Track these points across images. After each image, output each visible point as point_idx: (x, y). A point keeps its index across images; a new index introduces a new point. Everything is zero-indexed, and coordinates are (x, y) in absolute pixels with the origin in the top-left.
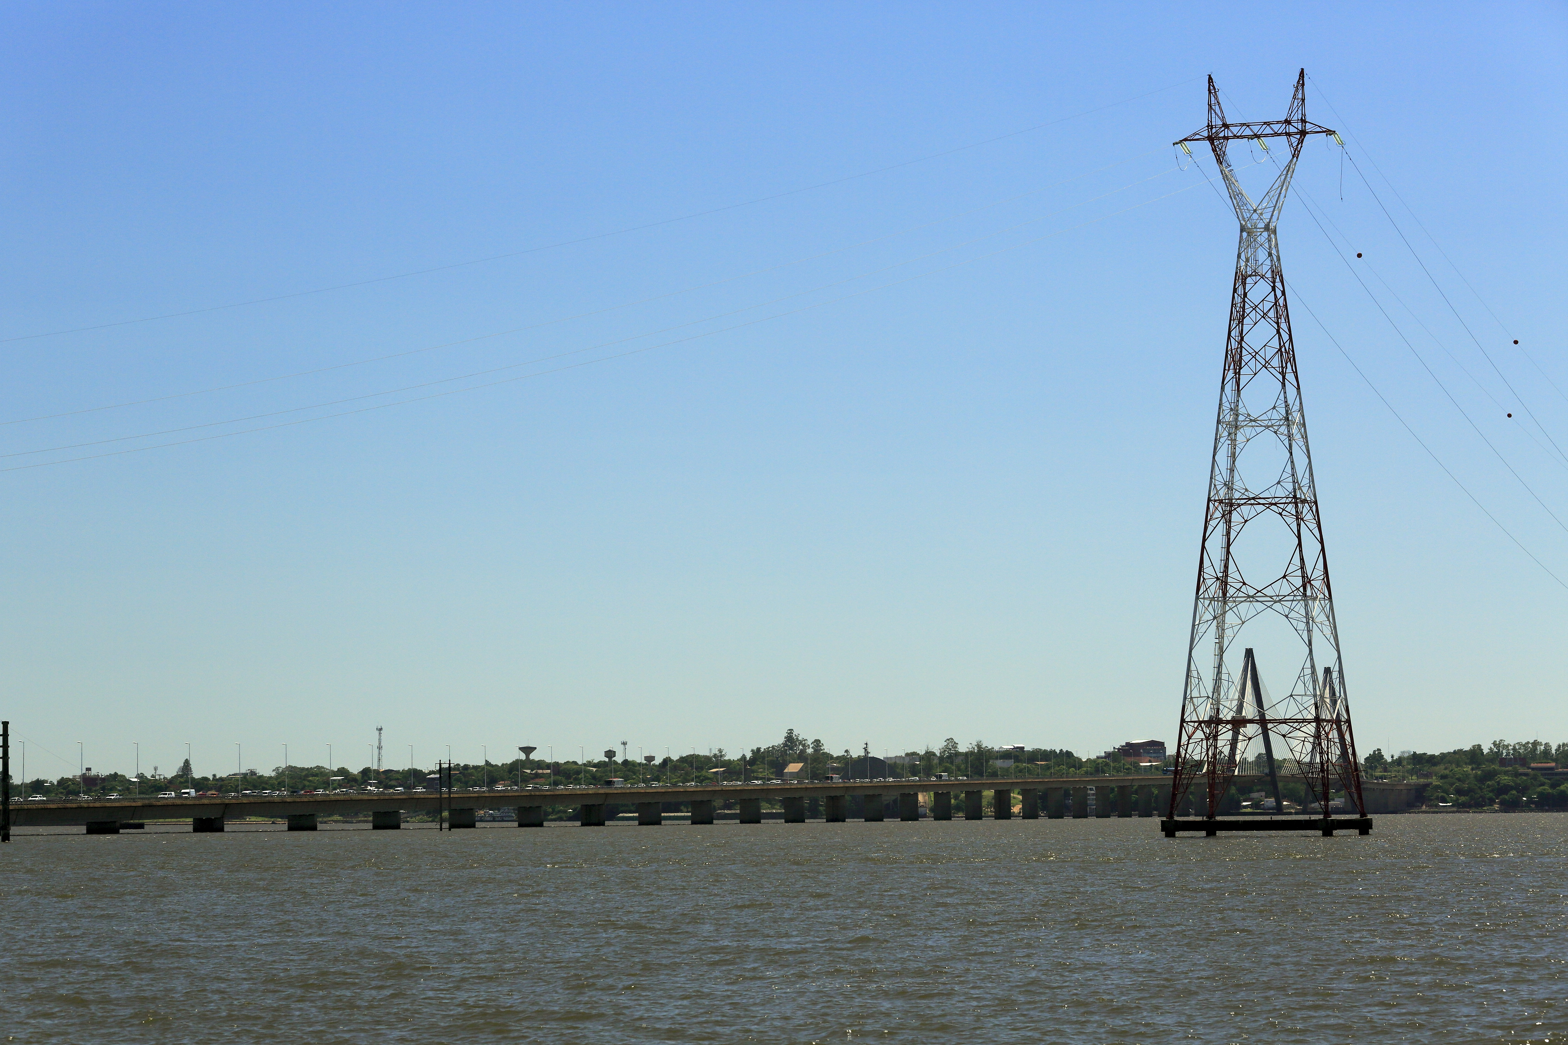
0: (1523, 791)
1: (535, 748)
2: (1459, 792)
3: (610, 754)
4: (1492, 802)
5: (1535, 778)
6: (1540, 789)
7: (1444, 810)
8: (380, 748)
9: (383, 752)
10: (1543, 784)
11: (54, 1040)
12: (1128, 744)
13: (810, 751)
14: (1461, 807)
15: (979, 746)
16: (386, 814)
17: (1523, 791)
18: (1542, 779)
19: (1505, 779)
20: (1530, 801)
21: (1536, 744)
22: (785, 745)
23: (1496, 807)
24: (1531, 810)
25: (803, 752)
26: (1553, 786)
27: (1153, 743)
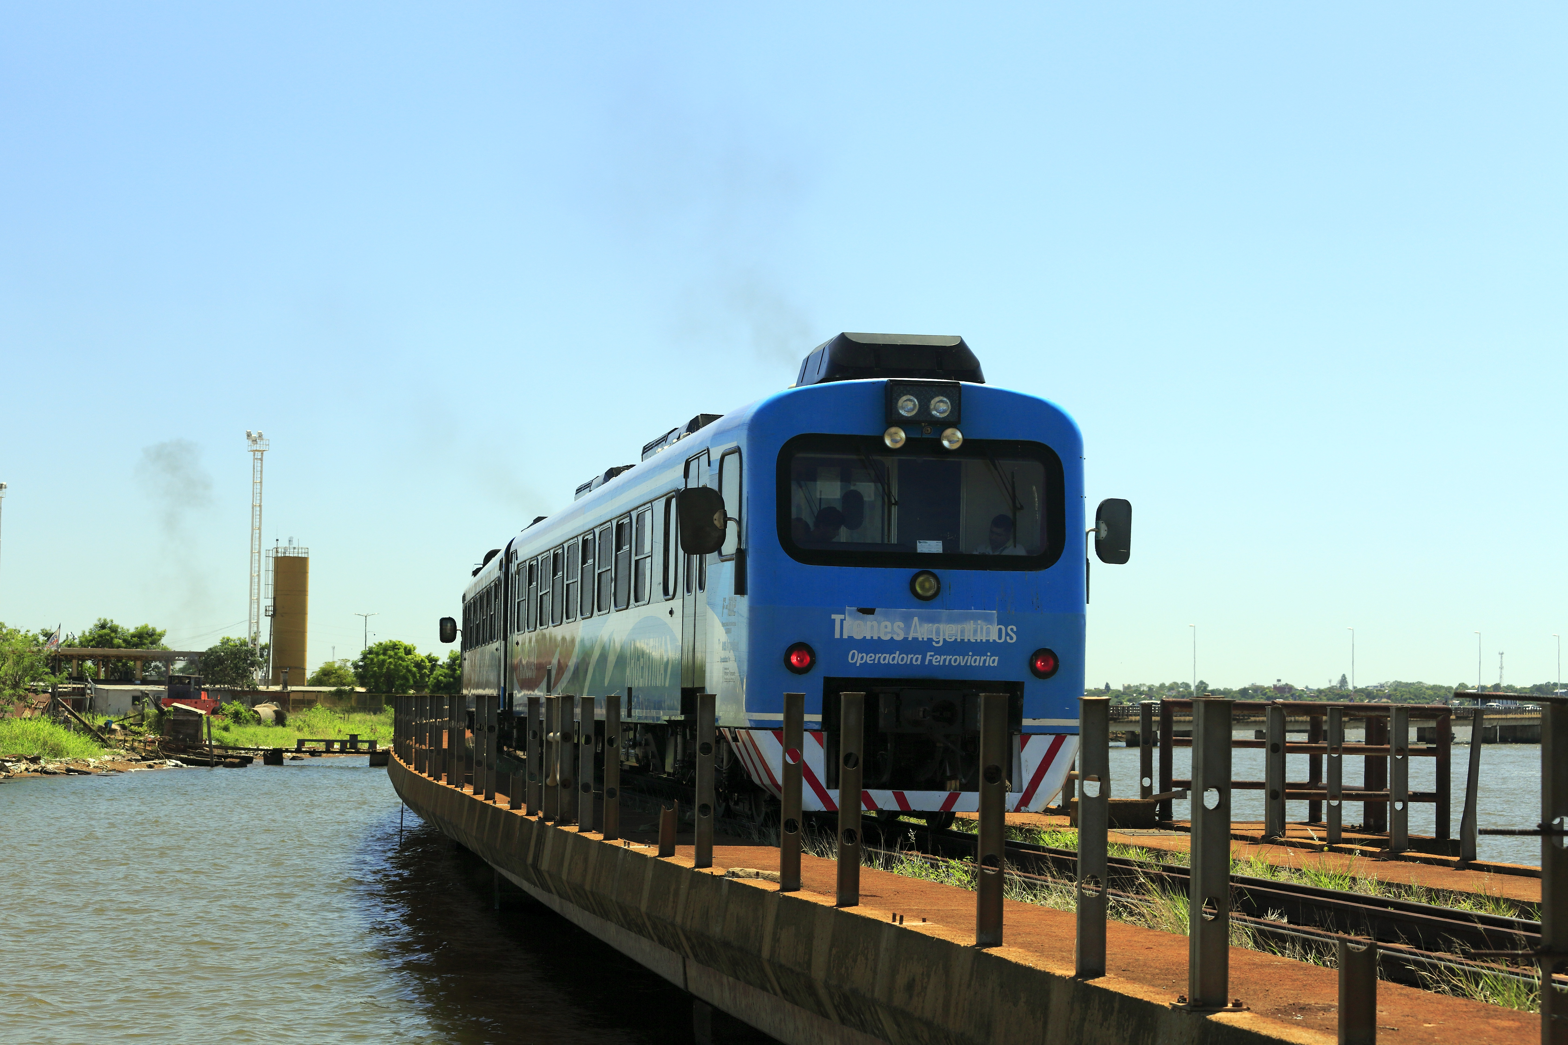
1: (1344, 676)
3: (1344, 680)
9: (1504, 671)
15: (1344, 680)
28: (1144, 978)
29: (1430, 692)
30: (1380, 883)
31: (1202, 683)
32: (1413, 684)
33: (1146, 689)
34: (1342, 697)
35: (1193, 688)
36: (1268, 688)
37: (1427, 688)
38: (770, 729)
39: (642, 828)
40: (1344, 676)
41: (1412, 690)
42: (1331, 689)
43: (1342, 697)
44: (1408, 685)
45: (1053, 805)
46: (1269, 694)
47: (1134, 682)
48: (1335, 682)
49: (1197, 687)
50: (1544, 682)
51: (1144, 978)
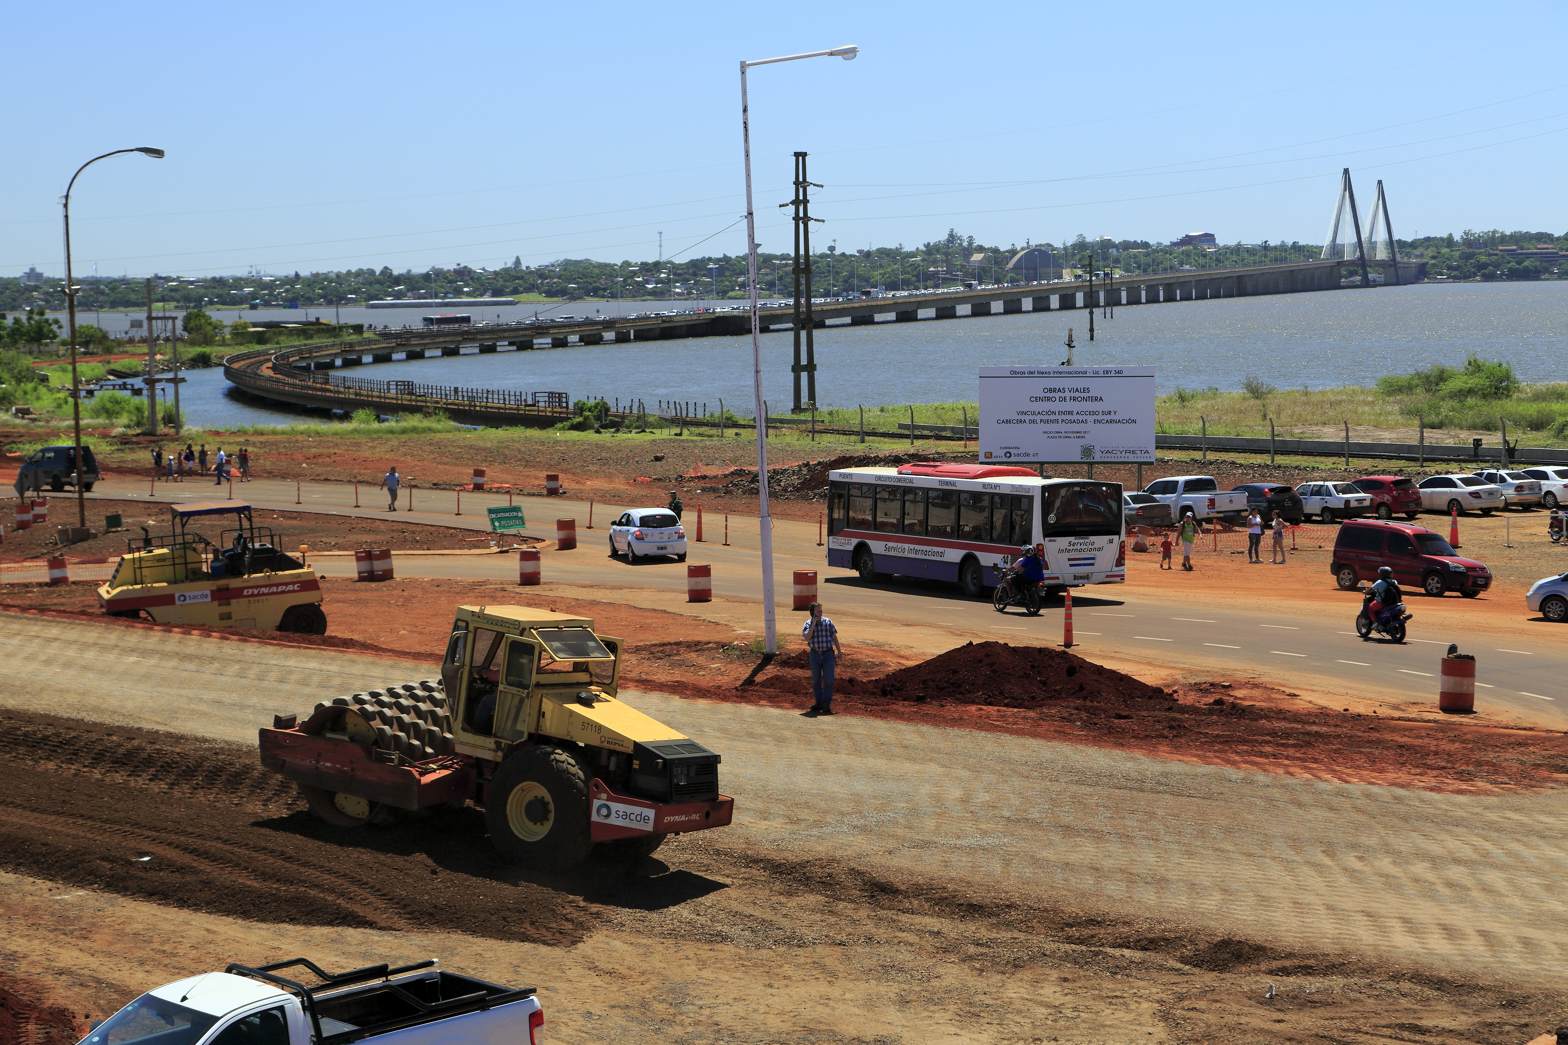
0: (1497, 266)
1: (518, 258)
2: (1450, 268)
3: (518, 262)
4: (1475, 275)
5: (1503, 257)
6: (1509, 265)
7: (1441, 281)
8: (661, 246)
9: (663, 249)
10: (1509, 262)
11: (1249, 1038)
12: (1187, 236)
13: (965, 244)
14: (1456, 279)
15: (518, 262)
16: (1013, 301)
17: (1497, 266)
18: (1508, 258)
19: (1483, 259)
20: (1503, 274)
21: (1494, 232)
22: (948, 241)
23: (1478, 278)
24: (1504, 280)
25: (961, 245)
26: (1519, 263)
27: (1206, 235)
28: (405, 540)
29: (596, 271)
30: (425, 319)
31: (386, 268)
32: (581, 261)
33: (333, 276)
34: (518, 278)
35: (378, 273)
36: (449, 271)
37: (594, 267)
38: (337, 809)
39: (146, 859)
40: (518, 258)
41: (581, 270)
42: (506, 270)
43: (518, 278)
44: (576, 263)
45: (388, 499)
46: (450, 278)
47: (323, 269)
48: (510, 264)
49: (382, 273)
50: (699, 257)
51: (405, 540)
